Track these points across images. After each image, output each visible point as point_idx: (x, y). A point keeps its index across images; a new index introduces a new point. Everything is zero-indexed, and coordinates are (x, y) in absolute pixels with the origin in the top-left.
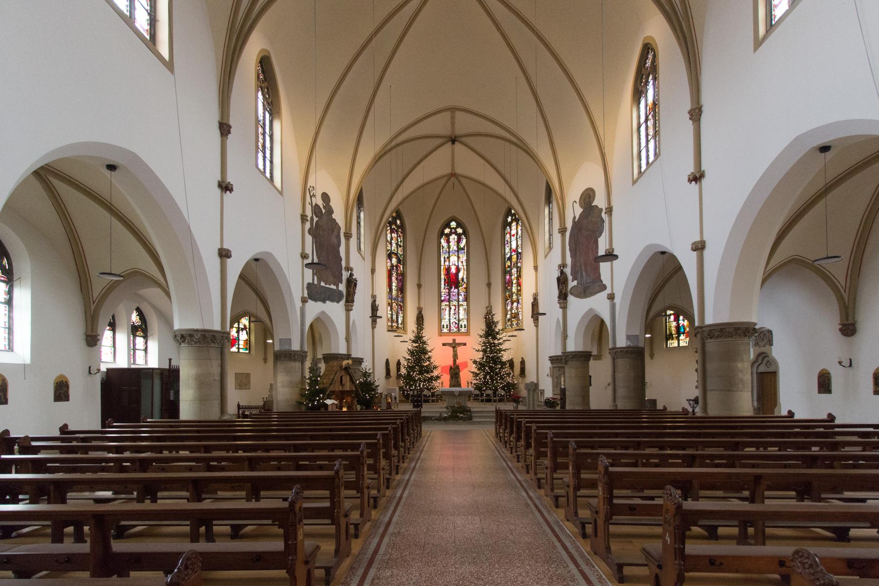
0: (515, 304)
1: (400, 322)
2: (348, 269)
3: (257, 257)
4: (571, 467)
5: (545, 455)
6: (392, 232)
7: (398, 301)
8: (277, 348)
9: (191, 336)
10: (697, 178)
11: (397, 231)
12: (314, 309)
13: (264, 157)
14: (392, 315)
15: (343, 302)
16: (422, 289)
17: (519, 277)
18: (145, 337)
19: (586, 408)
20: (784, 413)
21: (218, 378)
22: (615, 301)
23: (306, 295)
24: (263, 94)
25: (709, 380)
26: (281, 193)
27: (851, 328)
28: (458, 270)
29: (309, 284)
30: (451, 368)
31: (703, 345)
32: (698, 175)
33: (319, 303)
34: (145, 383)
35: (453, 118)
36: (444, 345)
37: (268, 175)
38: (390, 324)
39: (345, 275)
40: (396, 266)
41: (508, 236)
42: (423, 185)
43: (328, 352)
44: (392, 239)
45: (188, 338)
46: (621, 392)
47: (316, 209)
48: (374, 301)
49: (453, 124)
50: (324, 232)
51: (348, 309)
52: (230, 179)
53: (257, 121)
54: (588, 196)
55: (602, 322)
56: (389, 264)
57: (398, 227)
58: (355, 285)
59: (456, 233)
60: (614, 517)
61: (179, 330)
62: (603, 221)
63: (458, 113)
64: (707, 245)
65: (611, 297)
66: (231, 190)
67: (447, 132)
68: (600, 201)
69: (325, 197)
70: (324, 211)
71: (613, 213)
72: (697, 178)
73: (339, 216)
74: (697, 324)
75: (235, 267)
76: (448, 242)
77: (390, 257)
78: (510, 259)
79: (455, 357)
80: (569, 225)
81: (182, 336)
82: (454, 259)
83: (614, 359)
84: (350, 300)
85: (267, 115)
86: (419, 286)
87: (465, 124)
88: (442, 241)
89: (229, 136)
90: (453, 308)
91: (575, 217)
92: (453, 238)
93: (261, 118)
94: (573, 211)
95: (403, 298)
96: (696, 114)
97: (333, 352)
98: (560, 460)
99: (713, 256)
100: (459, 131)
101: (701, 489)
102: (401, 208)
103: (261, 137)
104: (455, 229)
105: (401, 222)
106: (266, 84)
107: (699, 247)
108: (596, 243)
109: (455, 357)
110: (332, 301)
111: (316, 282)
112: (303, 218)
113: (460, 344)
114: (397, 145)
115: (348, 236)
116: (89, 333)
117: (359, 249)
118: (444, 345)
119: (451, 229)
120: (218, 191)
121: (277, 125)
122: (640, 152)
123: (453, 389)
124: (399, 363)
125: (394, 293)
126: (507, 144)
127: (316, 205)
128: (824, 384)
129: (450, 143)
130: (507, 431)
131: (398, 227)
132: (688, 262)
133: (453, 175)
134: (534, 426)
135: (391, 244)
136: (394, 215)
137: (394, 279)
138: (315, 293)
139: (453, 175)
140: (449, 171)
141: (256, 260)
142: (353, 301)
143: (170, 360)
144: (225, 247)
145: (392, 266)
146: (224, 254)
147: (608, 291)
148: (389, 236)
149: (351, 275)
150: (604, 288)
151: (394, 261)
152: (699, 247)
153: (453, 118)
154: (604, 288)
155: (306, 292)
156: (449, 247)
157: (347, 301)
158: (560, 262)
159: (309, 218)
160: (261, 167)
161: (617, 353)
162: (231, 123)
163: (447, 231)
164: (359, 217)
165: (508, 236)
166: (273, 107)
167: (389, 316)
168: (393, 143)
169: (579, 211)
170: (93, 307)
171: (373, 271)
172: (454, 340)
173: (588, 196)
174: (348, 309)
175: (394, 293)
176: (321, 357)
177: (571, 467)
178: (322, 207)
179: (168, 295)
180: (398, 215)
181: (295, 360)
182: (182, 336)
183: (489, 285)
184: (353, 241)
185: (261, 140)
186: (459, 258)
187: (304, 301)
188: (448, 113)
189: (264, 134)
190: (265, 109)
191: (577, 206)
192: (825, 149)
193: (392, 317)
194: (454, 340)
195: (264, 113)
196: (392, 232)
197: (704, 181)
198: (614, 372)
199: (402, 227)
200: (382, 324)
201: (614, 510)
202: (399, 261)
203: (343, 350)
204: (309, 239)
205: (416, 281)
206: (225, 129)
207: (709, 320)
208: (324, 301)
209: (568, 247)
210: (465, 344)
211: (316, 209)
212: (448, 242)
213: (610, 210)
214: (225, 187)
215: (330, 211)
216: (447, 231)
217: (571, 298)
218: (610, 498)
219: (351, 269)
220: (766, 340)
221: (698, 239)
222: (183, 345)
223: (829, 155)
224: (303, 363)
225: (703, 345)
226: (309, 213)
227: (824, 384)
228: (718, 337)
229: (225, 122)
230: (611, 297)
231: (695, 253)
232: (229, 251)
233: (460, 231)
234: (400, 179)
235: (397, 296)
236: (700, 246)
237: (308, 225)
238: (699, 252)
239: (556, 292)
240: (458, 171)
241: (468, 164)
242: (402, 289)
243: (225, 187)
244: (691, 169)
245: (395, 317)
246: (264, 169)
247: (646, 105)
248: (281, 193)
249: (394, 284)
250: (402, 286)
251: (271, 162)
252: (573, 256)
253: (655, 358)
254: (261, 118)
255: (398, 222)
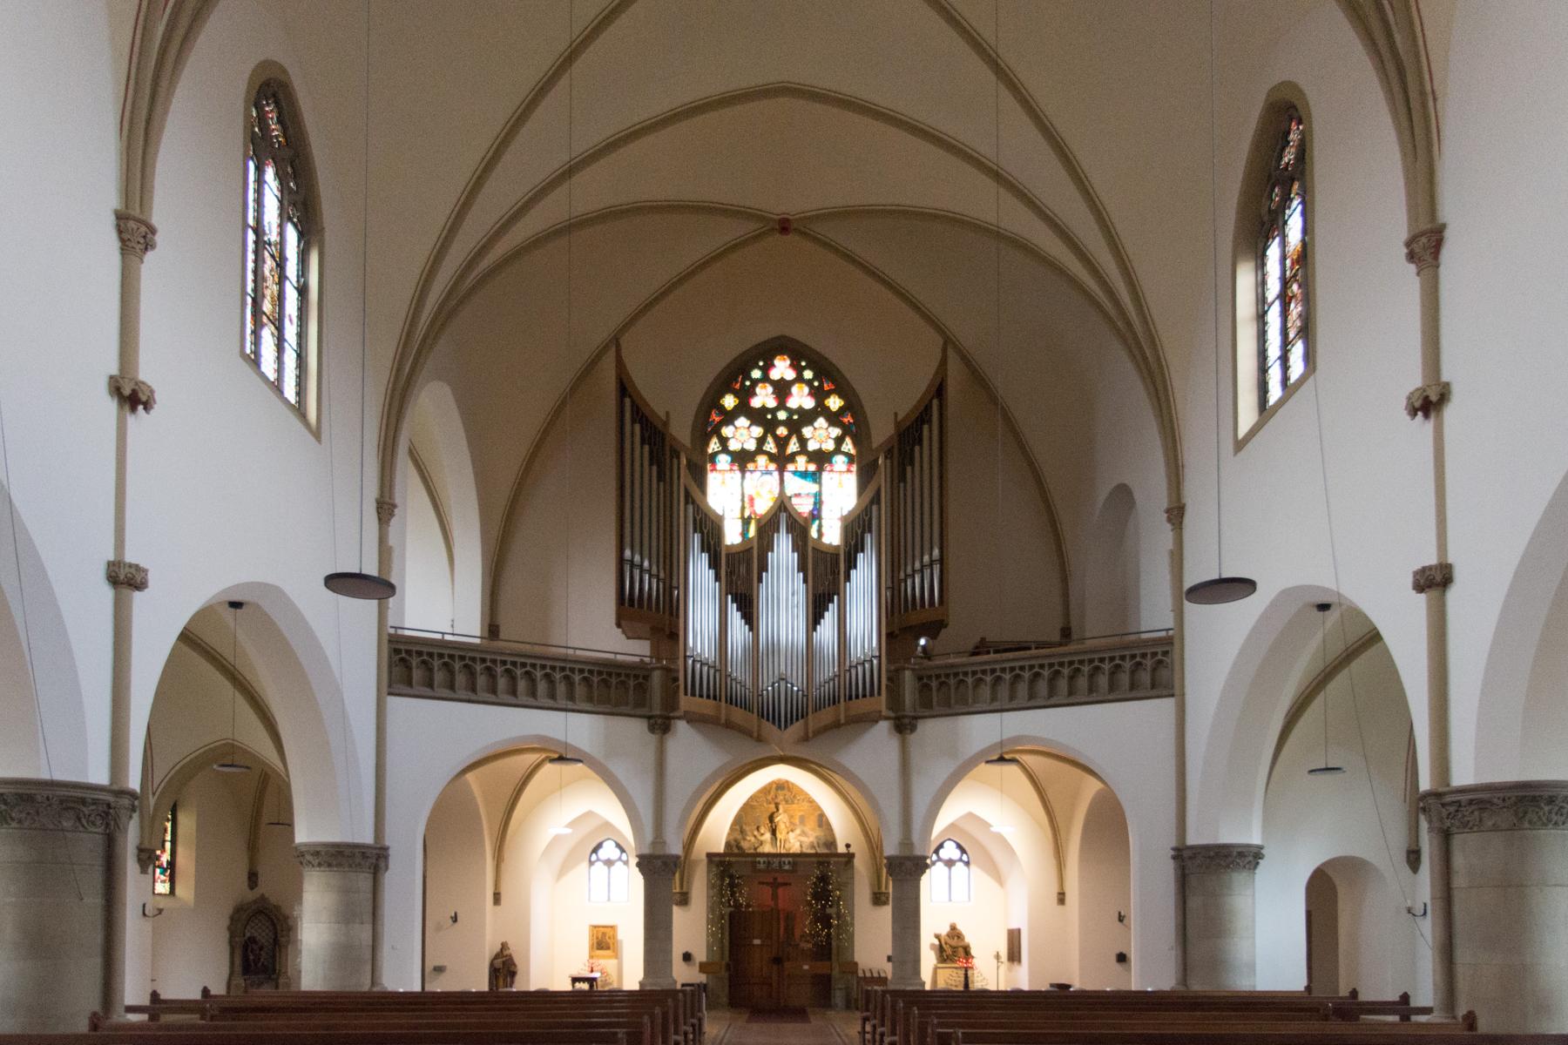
3: (236, 598)
10: (1429, 404)
19: (907, 853)
20: (1344, 991)
32: (1434, 398)
37: (290, 392)
52: (148, 372)
53: (245, 225)
64: (1459, 575)
66: (147, 406)
72: (1429, 404)
74: (1425, 784)
75: (157, 626)
85: (292, 234)
89: (149, 255)
93: (272, 235)
96: (1426, 246)
99: (1475, 609)
101: (641, 666)
116: (146, 845)
122: (1263, 370)
132: (1402, 624)
141: (236, 605)
144: (130, 557)
146: (125, 579)
152: (1434, 581)
162: (155, 220)
189: (282, 278)
190: (284, 217)
195: (281, 226)
197: (1450, 412)
206: (134, 234)
207: (1464, 774)
214: (131, 397)
221: (1431, 559)
229: (136, 212)
231: (1423, 596)
236: (1439, 578)
238: (1434, 593)
243: (131, 397)
244: (1414, 380)
246: (280, 370)
247: (1283, 258)
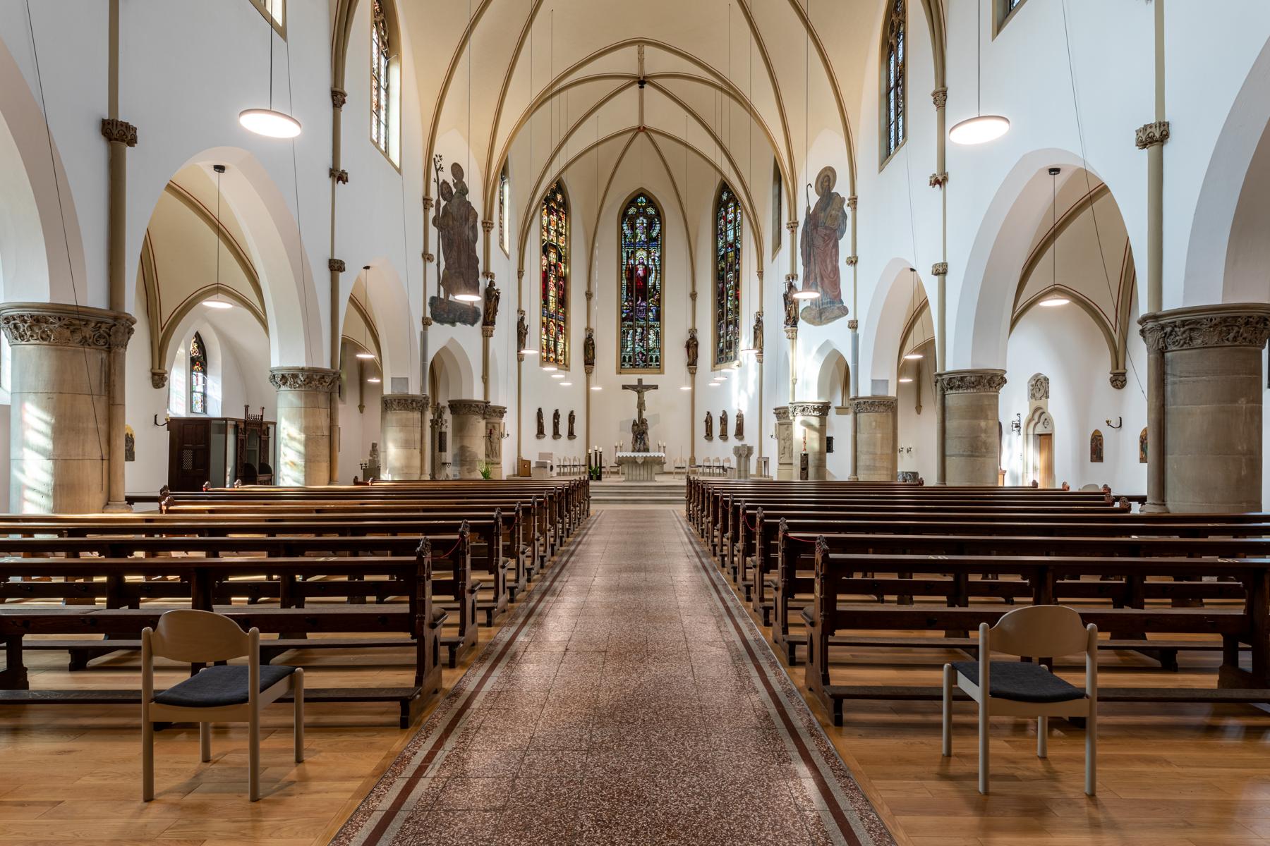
0: (731, 327)
1: (559, 351)
2: (487, 274)
4: (817, 587)
5: (807, 586)
6: (550, 212)
7: (556, 319)
8: (387, 391)
9: (295, 376)
10: (940, 181)
11: (557, 211)
12: (441, 335)
13: (379, 122)
14: (548, 340)
15: (479, 324)
16: (593, 301)
17: (737, 286)
18: (205, 372)
21: (326, 433)
22: (858, 331)
23: (429, 315)
24: (378, 33)
25: (949, 443)
26: (399, 171)
27: (1121, 378)
28: (647, 271)
29: (433, 298)
30: (635, 424)
31: (944, 396)
32: (940, 179)
33: (447, 326)
34: (215, 438)
35: (641, 53)
36: (625, 387)
37: (383, 147)
38: (544, 354)
39: (483, 283)
40: (555, 266)
41: (722, 222)
42: (598, 144)
43: (458, 398)
44: (549, 223)
45: (290, 381)
46: (864, 460)
47: (444, 189)
48: (522, 319)
49: (641, 61)
50: (455, 226)
51: (487, 335)
54: (826, 179)
55: (841, 357)
56: (545, 262)
57: (560, 205)
58: (497, 298)
59: (645, 215)
60: (837, 632)
61: (278, 369)
62: (845, 216)
63: (647, 49)
65: (854, 325)
67: (634, 71)
68: (841, 188)
69: (457, 170)
70: (454, 190)
71: (858, 206)
72: (940, 181)
73: (475, 198)
76: (633, 228)
77: (545, 250)
78: (724, 257)
79: (641, 406)
80: (801, 218)
81: (283, 376)
82: (641, 254)
83: (856, 414)
84: (489, 322)
85: (383, 59)
86: (589, 295)
87: (658, 62)
88: (625, 227)
90: (639, 330)
91: (809, 208)
92: (641, 220)
94: (807, 199)
95: (564, 314)
97: (465, 397)
98: (800, 575)
100: (648, 71)
102: (564, 176)
103: (375, 93)
104: (645, 208)
105: (564, 197)
106: (381, 17)
107: (941, 271)
108: (836, 246)
109: (641, 406)
110: (464, 322)
111: (442, 296)
112: (426, 201)
113: (648, 387)
114: (560, 91)
115: (488, 226)
117: (502, 242)
118: (625, 387)
119: (638, 208)
120: (329, 181)
121: (395, 72)
123: (636, 454)
124: (556, 415)
125: (552, 306)
126: (719, 92)
127: (444, 182)
128: (1097, 453)
129: (637, 86)
130: (729, 534)
131: (560, 205)
133: (642, 129)
134: (783, 524)
135: (548, 231)
136: (554, 186)
137: (551, 285)
138: (442, 312)
139: (642, 129)
140: (635, 123)
142: (493, 323)
143: (247, 407)
145: (549, 265)
147: (850, 317)
148: (545, 218)
149: (492, 284)
150: (845, 311)
151: (553, 257)
152: (941, 271)
153: (641, 53)
154: (845, 311)
155: (428, 309)
156: (635, 236)
157: (485, 323)
158: (788, 272)
159: (434, 203)
160: (375, 138)
161: (860, 406)
163: (632, 211)
164: (502, 193)
165: (722, 222)
166: (389, 46)
167: (545, 342)
168: (557, 88)
169: (815, 198)
170: (161, 335)
171: (520, 273)
172: (640, 381)
173: (826, 179)
174: (487, 335)
175: (552, 306)
176: (447, 404)
177: (817, 587)
178: (451, 184)
179: (264, 324)
180: (559, 187)
181: (413, 409)
182: (283, 376)
183: (694, 296)
184: (494, 233)
185: (375, 99)
186: (649, 253)
187: (426, 323)
188: (635, 48)
191: (812, 191)
192: (1055, 171)
193: (547, 345)
194: (640, 381)
196: (550, 212)
197: (948, 185)
198: (856, 432)
199: (565, 205)
200: (531, 352)
201: (834, 620)
202: (560, 258)
203: (478, 395)
204: (434, 232)
205: (585, 289)
206: (338, 98)
208: (453, 323)
209: (799, 251)
210: (656, 387)
211: (444, 189)
212: (633, 228)
213: (854, 201)
214: (338, 175)
215: (463, 191)
216: (632, 211)
217: (802, 324)
218: (828, 603)
219: (492, 276)
220: (1042, 391)
222: (283, 388)
223: (1060, 178)
224: (422, 413)
225: (944, 396)
226: (434, 195)
227: (1097, 453)
228: (959, 387)
230: (854, 325)
232: (342, 263)
233: (651, 211)
234: (562, 136)
235: (557, 312)
237: (432, 213)
239: (783, 316)
240: (649, 123)
241: (662, 114)
242: (563, 301)
243: (338, 175)
244: (934, 170)
245: (552, 343)
248: (399, 171)
249: (551, 293)
250: (564, 295)
251: (387, 126)
252: (807, 264)
253: (923, 410)
254: (375, 66)
255: (559, 197)
